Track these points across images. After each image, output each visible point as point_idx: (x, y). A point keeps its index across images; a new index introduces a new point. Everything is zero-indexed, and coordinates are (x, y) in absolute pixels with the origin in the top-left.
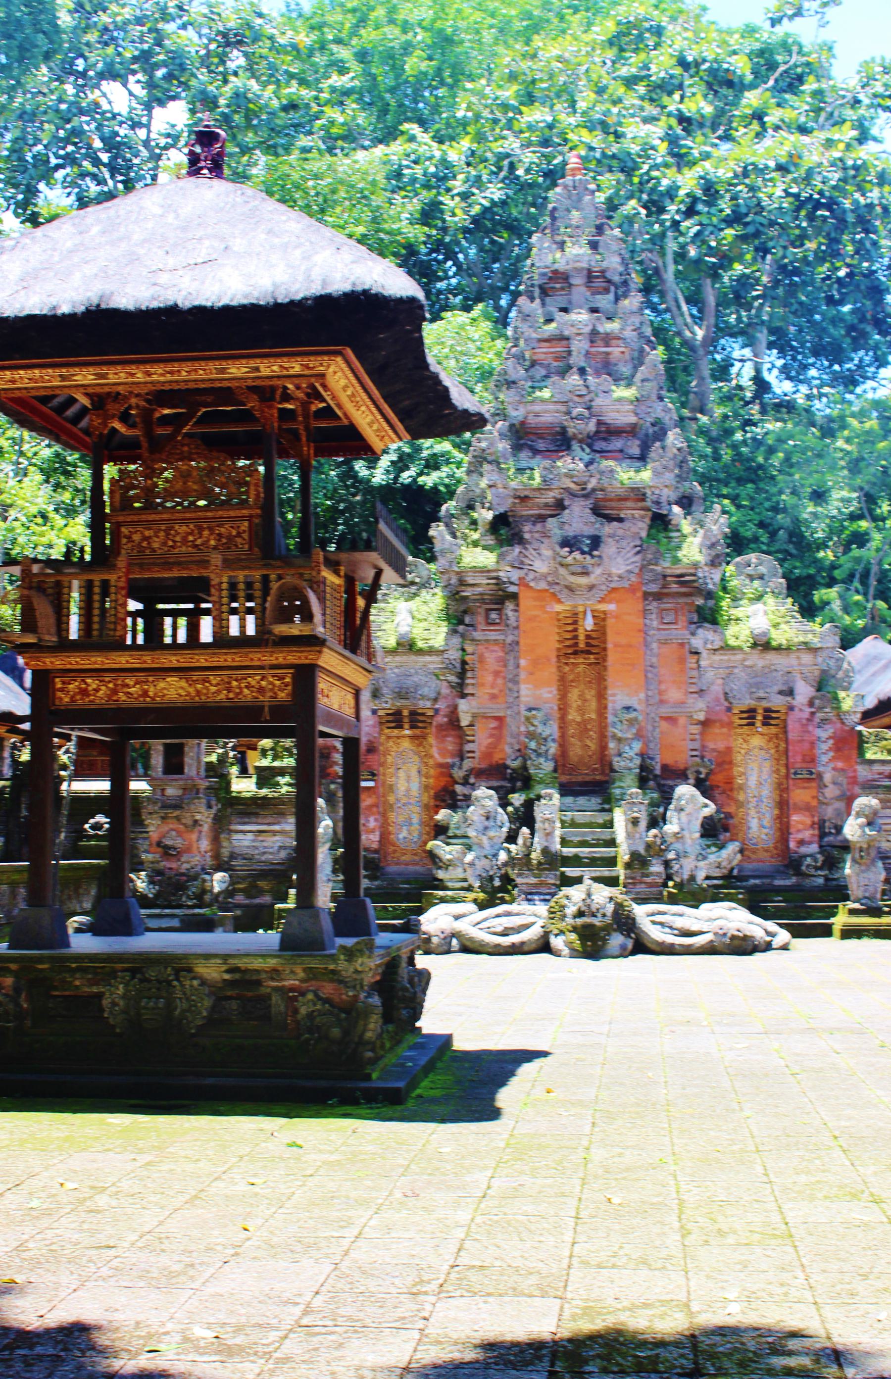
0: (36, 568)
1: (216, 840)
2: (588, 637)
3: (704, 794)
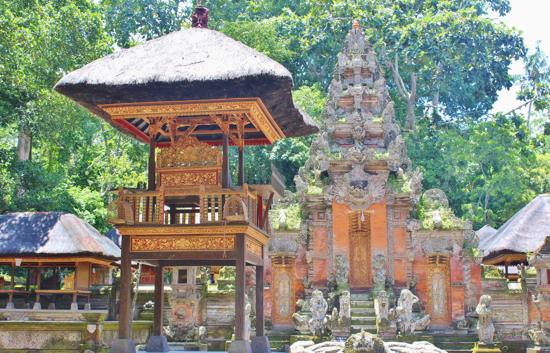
0: (125, 192)
1: (200, 312)
2: (362, 224)
3: (413, 293)
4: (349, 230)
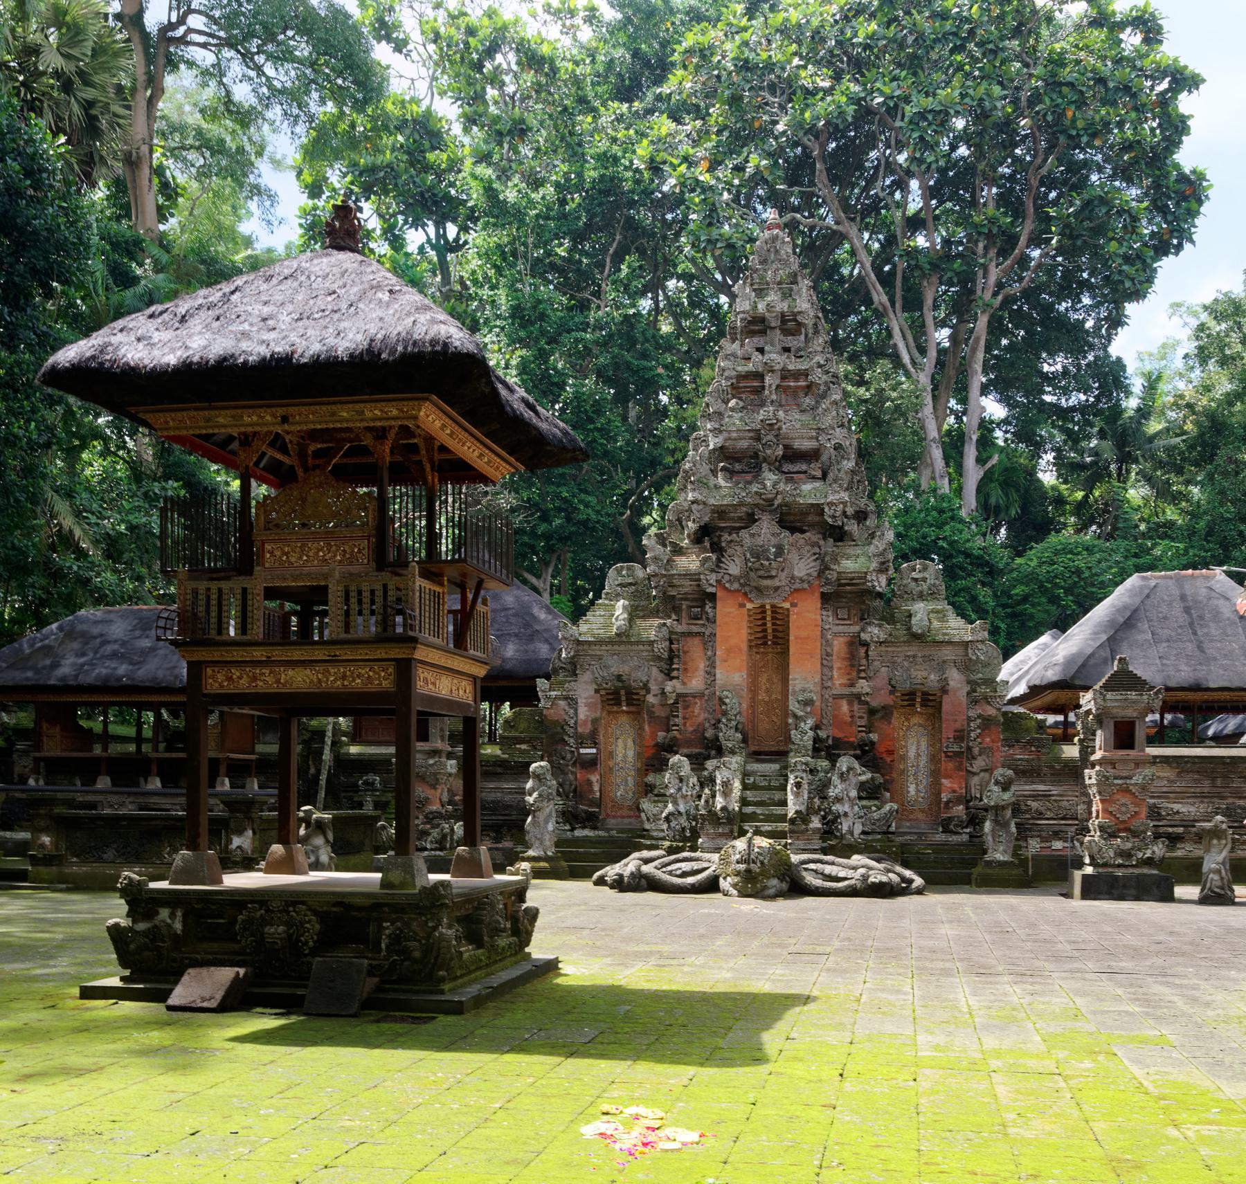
4: (750, 641)
